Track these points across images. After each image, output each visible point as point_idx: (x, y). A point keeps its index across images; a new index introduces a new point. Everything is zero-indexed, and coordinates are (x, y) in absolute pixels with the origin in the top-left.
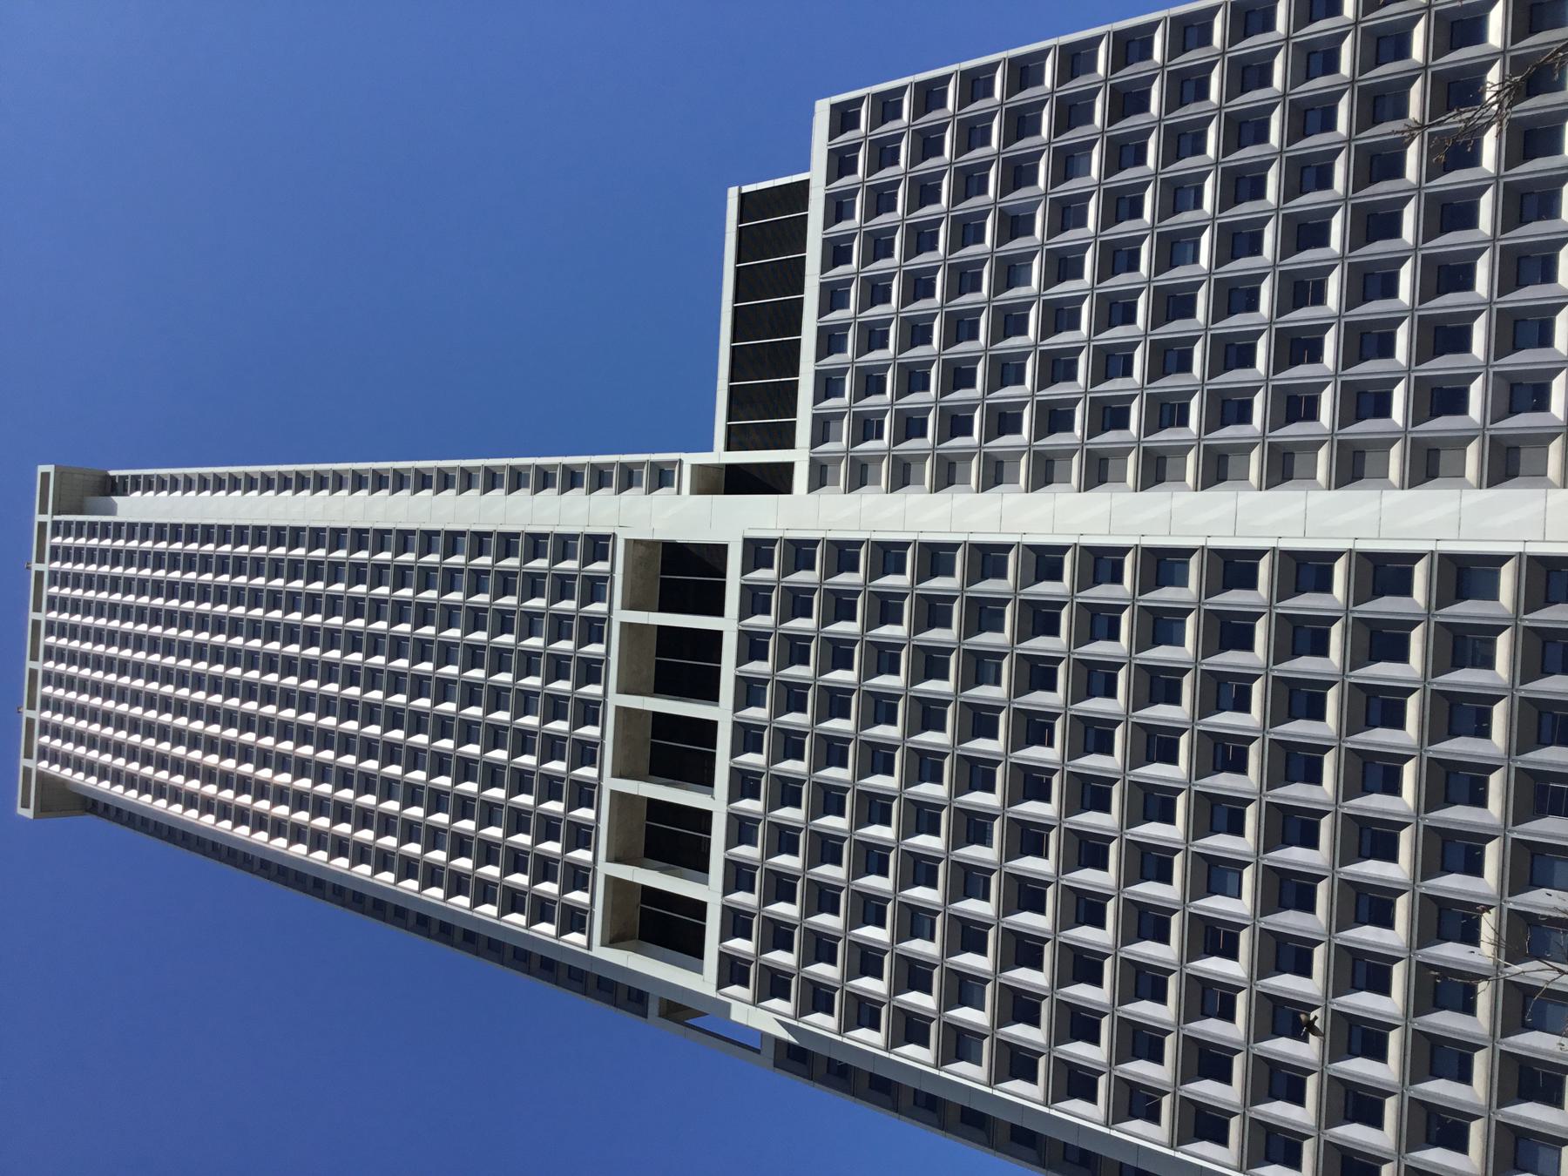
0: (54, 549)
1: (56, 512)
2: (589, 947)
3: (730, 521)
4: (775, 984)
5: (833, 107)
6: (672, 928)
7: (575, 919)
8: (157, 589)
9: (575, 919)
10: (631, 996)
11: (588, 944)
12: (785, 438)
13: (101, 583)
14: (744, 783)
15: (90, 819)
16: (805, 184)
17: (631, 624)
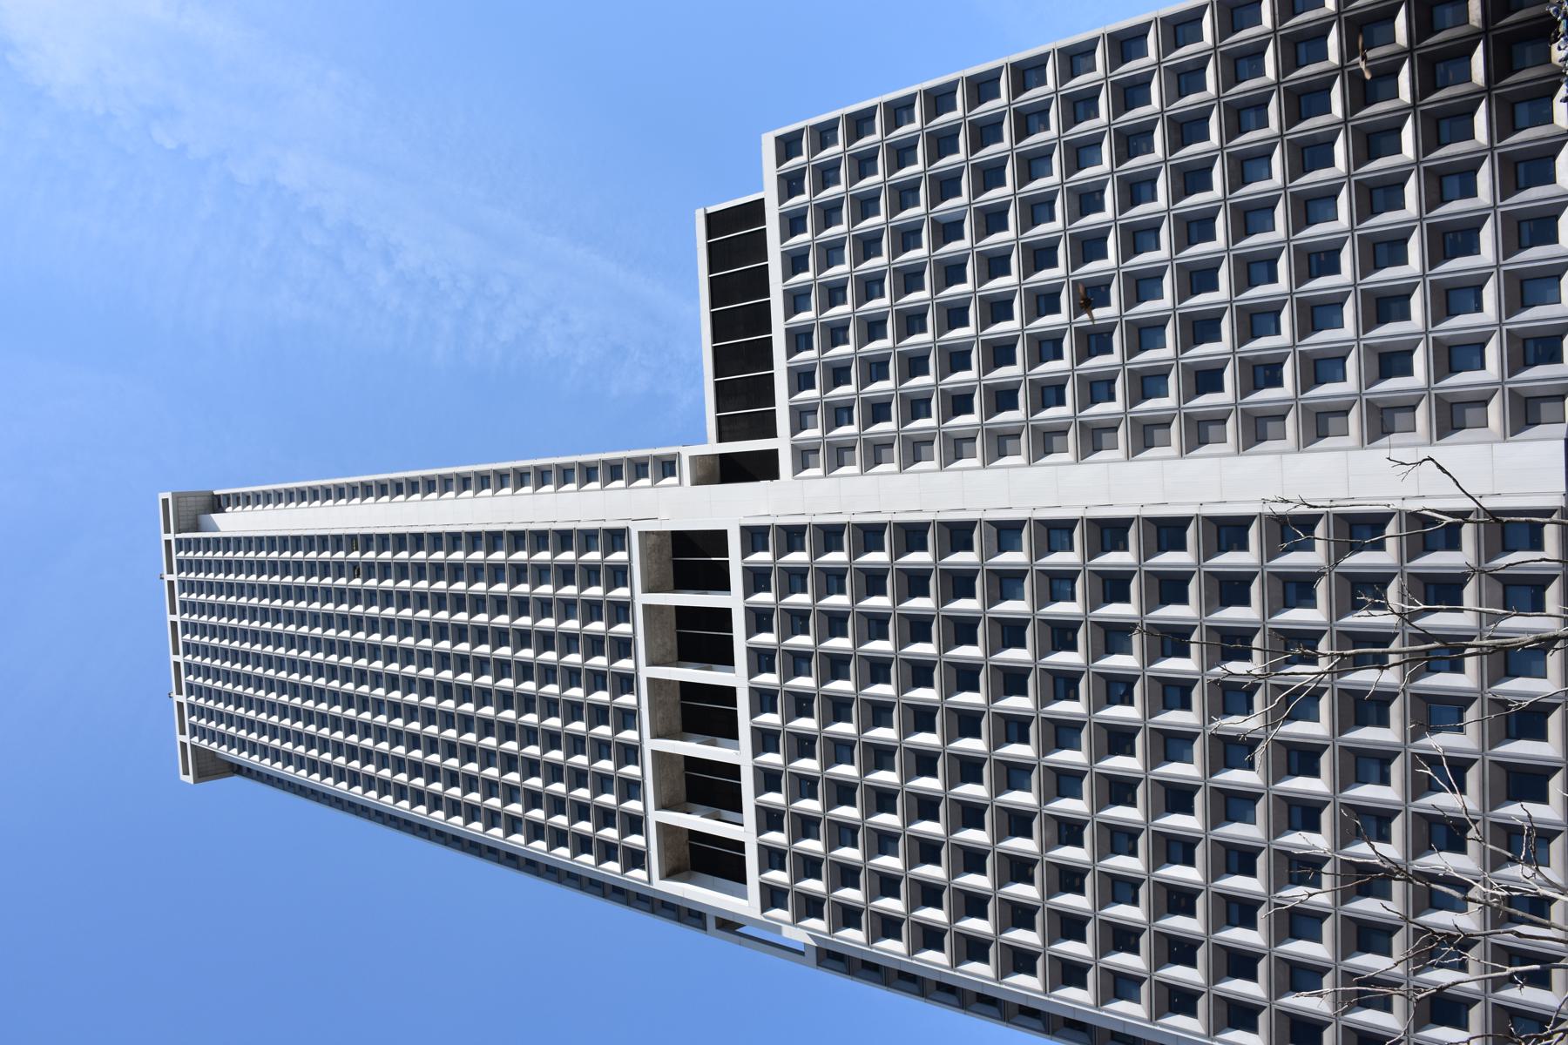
0: (180, 562)
1: (179, 531)
2: (650, 881)
3: (729, 509)
4: (810, 906)
5: (778, 139)
6: (721, 862)
7: (636, 859)
8: (264, 591)
9: (636, 859)
10: (693, 916)
11: (650, 878)
12: (767, 427)
13: (220, 588)
14: (757, 579)
15: (236, 780)
16: (760, 203)
17: (664, 754)
